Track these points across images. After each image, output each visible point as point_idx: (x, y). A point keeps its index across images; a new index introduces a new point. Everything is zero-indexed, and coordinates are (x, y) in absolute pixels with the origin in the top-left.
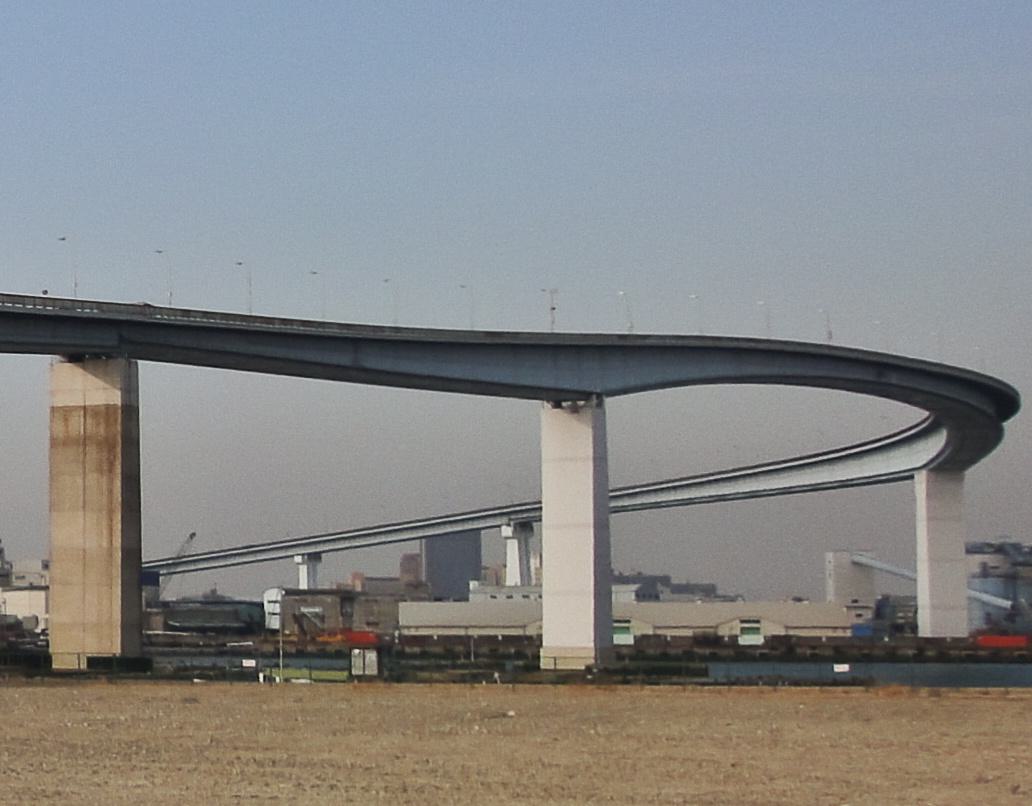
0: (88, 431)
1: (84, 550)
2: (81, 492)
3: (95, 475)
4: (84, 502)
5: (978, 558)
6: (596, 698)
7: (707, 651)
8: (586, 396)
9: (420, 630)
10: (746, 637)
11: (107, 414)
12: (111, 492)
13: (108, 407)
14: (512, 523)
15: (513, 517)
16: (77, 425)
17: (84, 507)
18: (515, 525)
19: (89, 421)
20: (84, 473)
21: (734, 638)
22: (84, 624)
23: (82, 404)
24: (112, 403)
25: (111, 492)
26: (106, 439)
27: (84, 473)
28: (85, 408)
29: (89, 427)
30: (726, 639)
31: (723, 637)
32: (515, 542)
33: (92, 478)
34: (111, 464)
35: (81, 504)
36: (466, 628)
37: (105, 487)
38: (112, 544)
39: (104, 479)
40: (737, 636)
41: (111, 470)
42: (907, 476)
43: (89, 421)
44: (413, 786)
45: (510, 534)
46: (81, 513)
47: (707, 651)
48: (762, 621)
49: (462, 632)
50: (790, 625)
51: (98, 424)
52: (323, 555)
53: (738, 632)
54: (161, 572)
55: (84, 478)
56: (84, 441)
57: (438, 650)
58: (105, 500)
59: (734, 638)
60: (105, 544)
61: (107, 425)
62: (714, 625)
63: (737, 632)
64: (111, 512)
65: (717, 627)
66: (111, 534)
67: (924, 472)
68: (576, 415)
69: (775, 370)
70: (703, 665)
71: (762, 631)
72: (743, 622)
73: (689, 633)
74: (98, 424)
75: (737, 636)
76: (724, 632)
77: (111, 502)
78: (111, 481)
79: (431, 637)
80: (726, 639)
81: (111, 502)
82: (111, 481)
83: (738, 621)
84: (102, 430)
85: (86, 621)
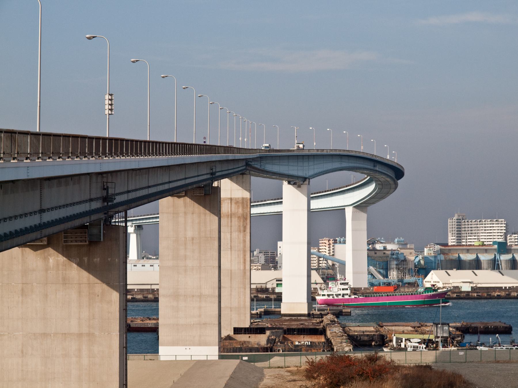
1: (231, 270)
3: (237, 233)
6: (410, 338)
7: (264, 296)
8: (305, 179)
11: (243, 203)
12: (244, 241)
13: (243, 199)
14: (133, 225)
17: (231, 248)
18: (135, 226)
19: (233, 205)
20: (231, 232)
21: (273, 289)
23: (229, 197)
24: (245, 197)
25: (244, 241)
26: (243, 215)
28: (231, 199)
30: (270, 289)
32: (135, 235)
33: (235, 235)
34: (245, 227)
36: (151, 285)
37: (242, 238)
38: (245, 268)
39: (242, 234)
41: (245, 231)
42: (341, 211)
43: (233, 205)
44: (337, 383)
45: (132, 231)
46: (229, 252)
47: (264, 296)
49: (148, 287)
55: (231, 235)
59: (273, 289)
60: (242, 267)
61: (243, 208)
62: (264, 282)
63: (275, 286)
64: (245, 251)
65: (266, 283)
67: (351, 207)
68: (299, 189)
70: (349, 310)
72: (277, 280)
76: (269, 286)
80: (270, 289)
83: (275, 280)
84: (240, 211)
85: (232, 306)
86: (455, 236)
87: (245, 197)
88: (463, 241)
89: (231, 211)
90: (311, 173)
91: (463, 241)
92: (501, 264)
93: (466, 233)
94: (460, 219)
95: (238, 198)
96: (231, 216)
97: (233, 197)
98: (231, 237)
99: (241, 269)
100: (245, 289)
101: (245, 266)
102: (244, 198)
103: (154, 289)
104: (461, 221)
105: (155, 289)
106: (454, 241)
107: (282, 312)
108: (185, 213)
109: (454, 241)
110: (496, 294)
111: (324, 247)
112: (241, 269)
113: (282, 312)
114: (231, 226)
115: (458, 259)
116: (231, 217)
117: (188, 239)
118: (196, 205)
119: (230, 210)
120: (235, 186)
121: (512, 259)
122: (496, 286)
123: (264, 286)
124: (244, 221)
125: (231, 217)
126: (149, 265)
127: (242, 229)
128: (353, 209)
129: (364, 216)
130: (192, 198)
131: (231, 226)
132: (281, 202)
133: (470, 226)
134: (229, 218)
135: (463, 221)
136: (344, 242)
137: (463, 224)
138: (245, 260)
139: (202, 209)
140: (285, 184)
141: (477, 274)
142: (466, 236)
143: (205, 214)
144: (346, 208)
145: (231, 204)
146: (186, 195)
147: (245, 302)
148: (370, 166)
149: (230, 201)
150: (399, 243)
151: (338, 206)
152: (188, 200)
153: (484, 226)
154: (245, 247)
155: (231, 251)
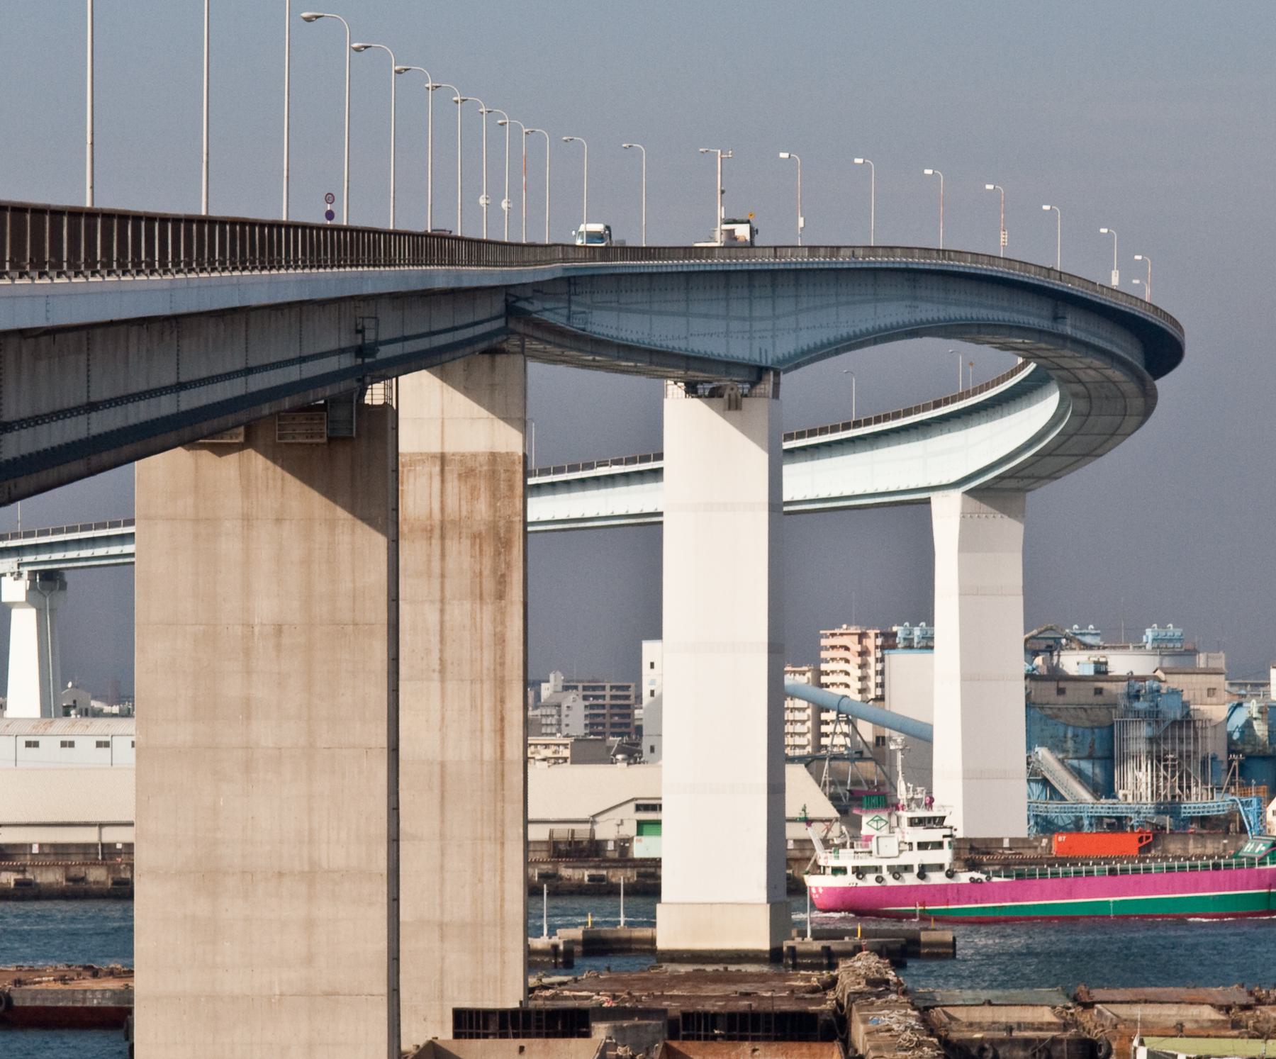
0: (449, 510)
1: (443, 765)
2: (435, 639)
3: (467, 605)
8: (757, 373)
9: (106, 830)
13: (493, 457)
14: (25, 571)
15: (27, 559)
17: (442, 671)
21: (623, 845)
23: (436, 448)
28: (443, 459)
29: (452, 502)
30: (611, 846)
32: (31, 613)
33: (459, 612)
34: (502, 581)
36: (101, 825)
37: (488, 628)
38: (502, 752)
39: (489, 610)
40: (630, 840)
43: (453, 485)
45: (21, 597)
46: (435, 685)
49: (89, 836)
51: (474, 495)
55: (442, 611)
57: (51, 877)
58: (488, 657)
59: (623, 845)
60: (489, 752)
61: (494, 495)
63: (630, 829)
64: (500, 682)
65: (592, 821)
66: (501, 731)
67: (957, 494)
68: (734, 414)
69: (929, 311)
70: (948, 936)
72: (639, 808)
74: (474, 495)
75: (630, 840)
76: (606, 831)
77: (501, 663)
78: (500, 619)
79: (25, 847)
80: (611, 846)
81: (501, 663)
82: (500, 619)
84: (482, 508)
87: (501, 448)
89: (442, 509)
90: (786, 346)
95: (474, 456)
96: (443, 530)
97: (449, 449)
98: (442, 623)
100: (503, 844)
101: (502, 746)
102: (500, 453)
105: (119, 846)
108: (247, 520)
113: (661, 945)
114: (443, 576)
116: (443, 537)
117: (257, 629)
118: (294, 485)
120: (459, 403)
123: (582, 831)
124: (500, 554)
125: (443, 537)
127: (489, 585)
128: (964, 503)
129: (1010, 531)
130: (276, 454)
131: (443, 576)
132: (657, 474)
134: (436, 541)
136: (927, 644)
138: (502, 719)
139: (316, 500)
140: (674, 392)
143: (332, 524)
144: (937, 500)
145: (443, 481)
146: (248, 443)
147: (503, 900)
148: (1034, 315)
149: (437, 469)
150: (1161, 646)
152: (257, 462)
154: (502, 664)
155: (443, 680)
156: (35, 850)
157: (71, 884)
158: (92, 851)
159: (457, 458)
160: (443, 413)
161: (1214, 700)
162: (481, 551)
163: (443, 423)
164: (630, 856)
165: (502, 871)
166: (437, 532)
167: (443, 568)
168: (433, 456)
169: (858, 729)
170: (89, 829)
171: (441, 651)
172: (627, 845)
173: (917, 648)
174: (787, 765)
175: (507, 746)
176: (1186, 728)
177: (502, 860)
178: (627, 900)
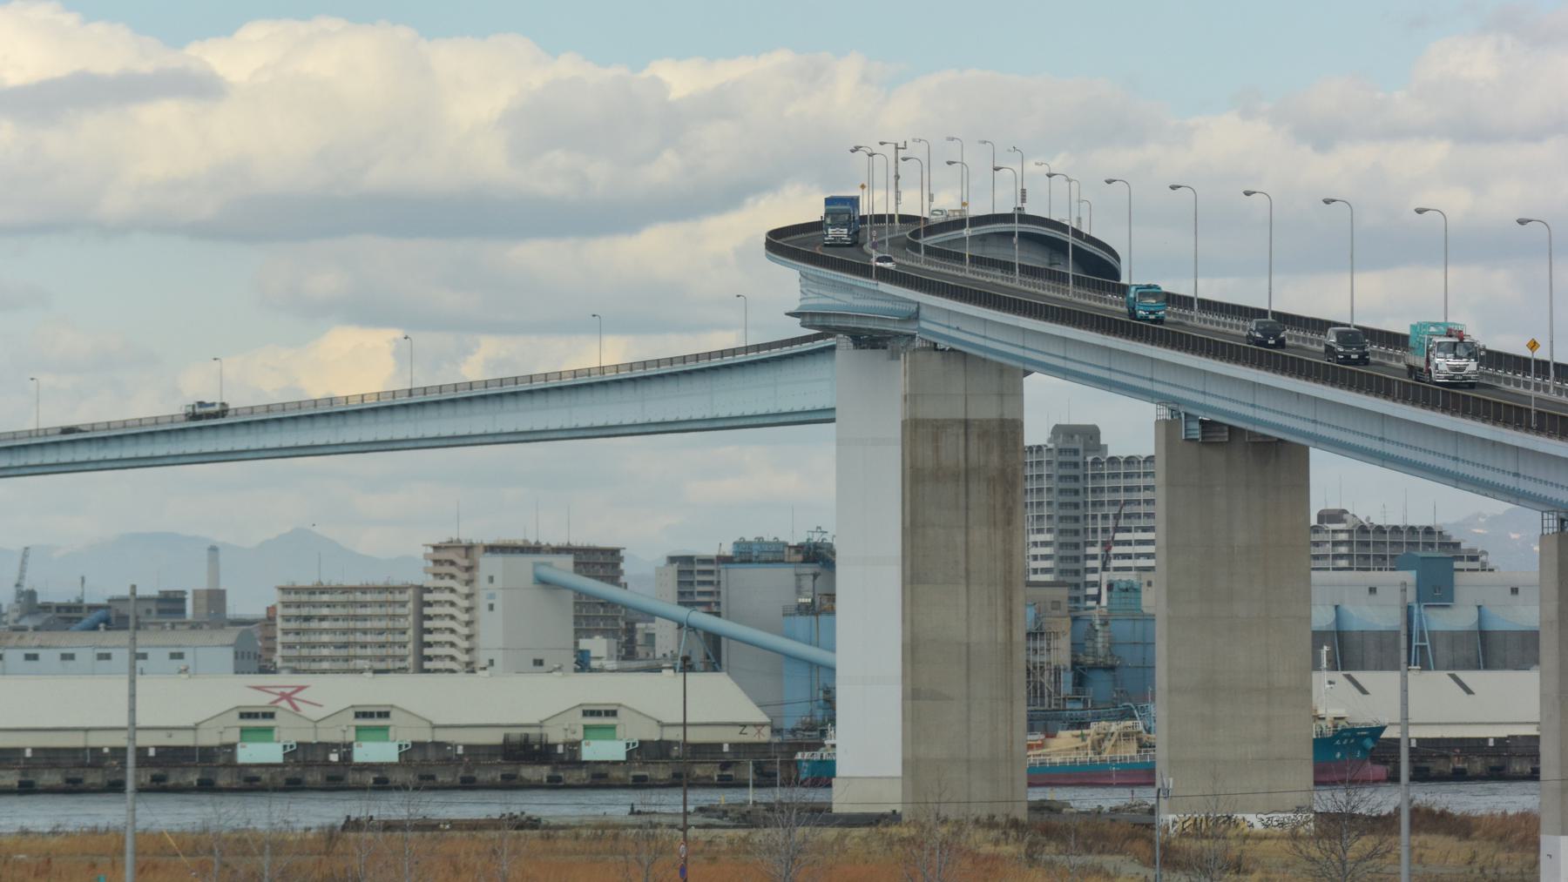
1: (968, 645)
4: (967, 571)
5: (676, 566)
9: (92, 735)
10: (250, 746)
16: (952, 451)
19: (973, 442)
20: (967, 527)
21: (573, 746)
22: (968, 761)
23: (961, 416)
27: (967, 527)
28: (966, 423)
31: (555, 746)
33: (979, 535)
35: (963, 573)
36: (87, 730)
38: (1011, 636)
40: (578, 743)
43: (974, 442)
46: (962, 589)
48: (621, 712)
50: (666, 720)
52: (657, 619)
53: (579, 736)
54: (664, 665)
55: (967, 534)
56: (966, 475)
59: (573, 746)
60: (1001, 636)
62: (536, 721)
71: (619, 732)
73: (496, 738)
75: (578, 743)
76: (556, 736)
80: (560, 749)
83: (579, 712)
84: (995, 459)
86: (1050, 531)
88: (1090, 551)
89: (966, 459)
91: (1090, 551)
92: (1434, 650)
93: (1105, 517)
94: (1076, 452)
95: (989, 421)
97: (971, 416)
98: (967, 543)
99: (999, 640)
100: (1012, 702)
101: (1011, 631)
102: (1006, 420)
103: (99, 750)
104: (1079, 459)
105: (106, 750)
106: (1047, 551)
107: (836, 809)
109: (1047, 551)
110: (1451, 766)
111: (447, 578)
112: (999, 640)
113: (836, 809)
114: (967, 508)
115: (1333, 628)
116: (967, 481)
117: (1236, 548)
119: (962, 456)
121: (1477, 629)
122: (1447, 735)
124: (1008, 492)
125: (967, 481)
126: (57, 653)
131: (967, 508)
133: (1122, 483)
134: (962, 483)
135: (1089, 459)
137: (1122, 471)
138: (1011, 612)
141: (1367, 688)
142: (1105, 530)
145: (967, 440)
147: (1012, 742)
149: (962, 431)
151: (818, 407)
153: (1122, 483)
154: (1010, 572)
155: (968, 584)
156: (28, 753)
157: (70, 785)
158: (81, 755)
159: (976, 423)
160: (966, 390)
161: (1058, 613)
162: (994, 489)
163: (966, 398)
164: (578, 758)
165: (1012, 722)
166: (962, 477)
167: (967, 503)
168: (959, 421)
169: (1334, 616)
170: (77, 733)
171: (967, 562)
172: (576, 748)
173: (755, 562)
174: (1538, 624)
175: (1015, 631)
176: (1040, 639)
177: (1012, 714)
178: (746, 777)
